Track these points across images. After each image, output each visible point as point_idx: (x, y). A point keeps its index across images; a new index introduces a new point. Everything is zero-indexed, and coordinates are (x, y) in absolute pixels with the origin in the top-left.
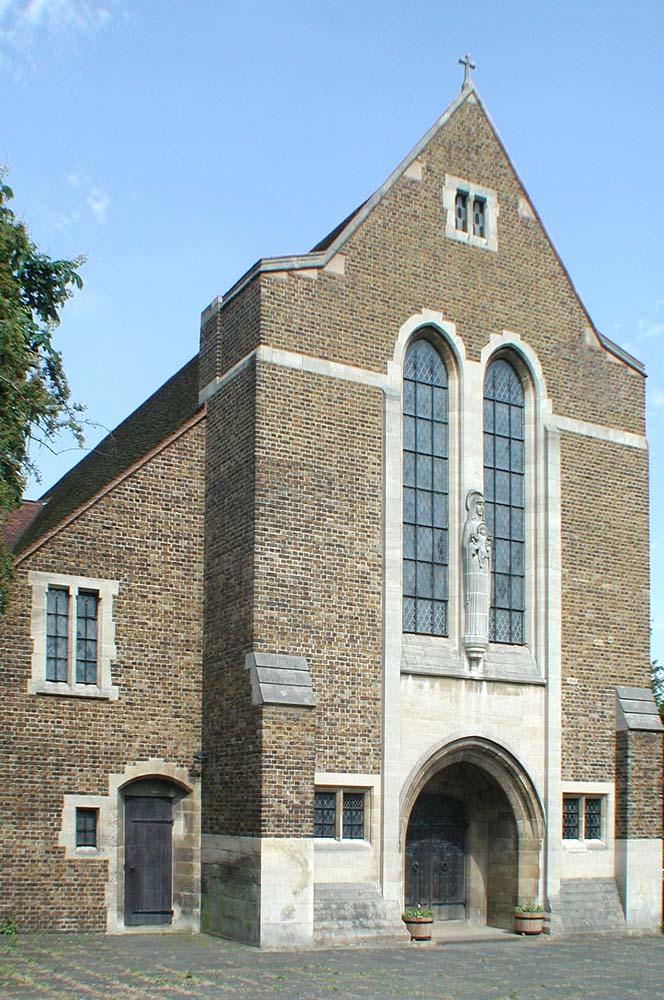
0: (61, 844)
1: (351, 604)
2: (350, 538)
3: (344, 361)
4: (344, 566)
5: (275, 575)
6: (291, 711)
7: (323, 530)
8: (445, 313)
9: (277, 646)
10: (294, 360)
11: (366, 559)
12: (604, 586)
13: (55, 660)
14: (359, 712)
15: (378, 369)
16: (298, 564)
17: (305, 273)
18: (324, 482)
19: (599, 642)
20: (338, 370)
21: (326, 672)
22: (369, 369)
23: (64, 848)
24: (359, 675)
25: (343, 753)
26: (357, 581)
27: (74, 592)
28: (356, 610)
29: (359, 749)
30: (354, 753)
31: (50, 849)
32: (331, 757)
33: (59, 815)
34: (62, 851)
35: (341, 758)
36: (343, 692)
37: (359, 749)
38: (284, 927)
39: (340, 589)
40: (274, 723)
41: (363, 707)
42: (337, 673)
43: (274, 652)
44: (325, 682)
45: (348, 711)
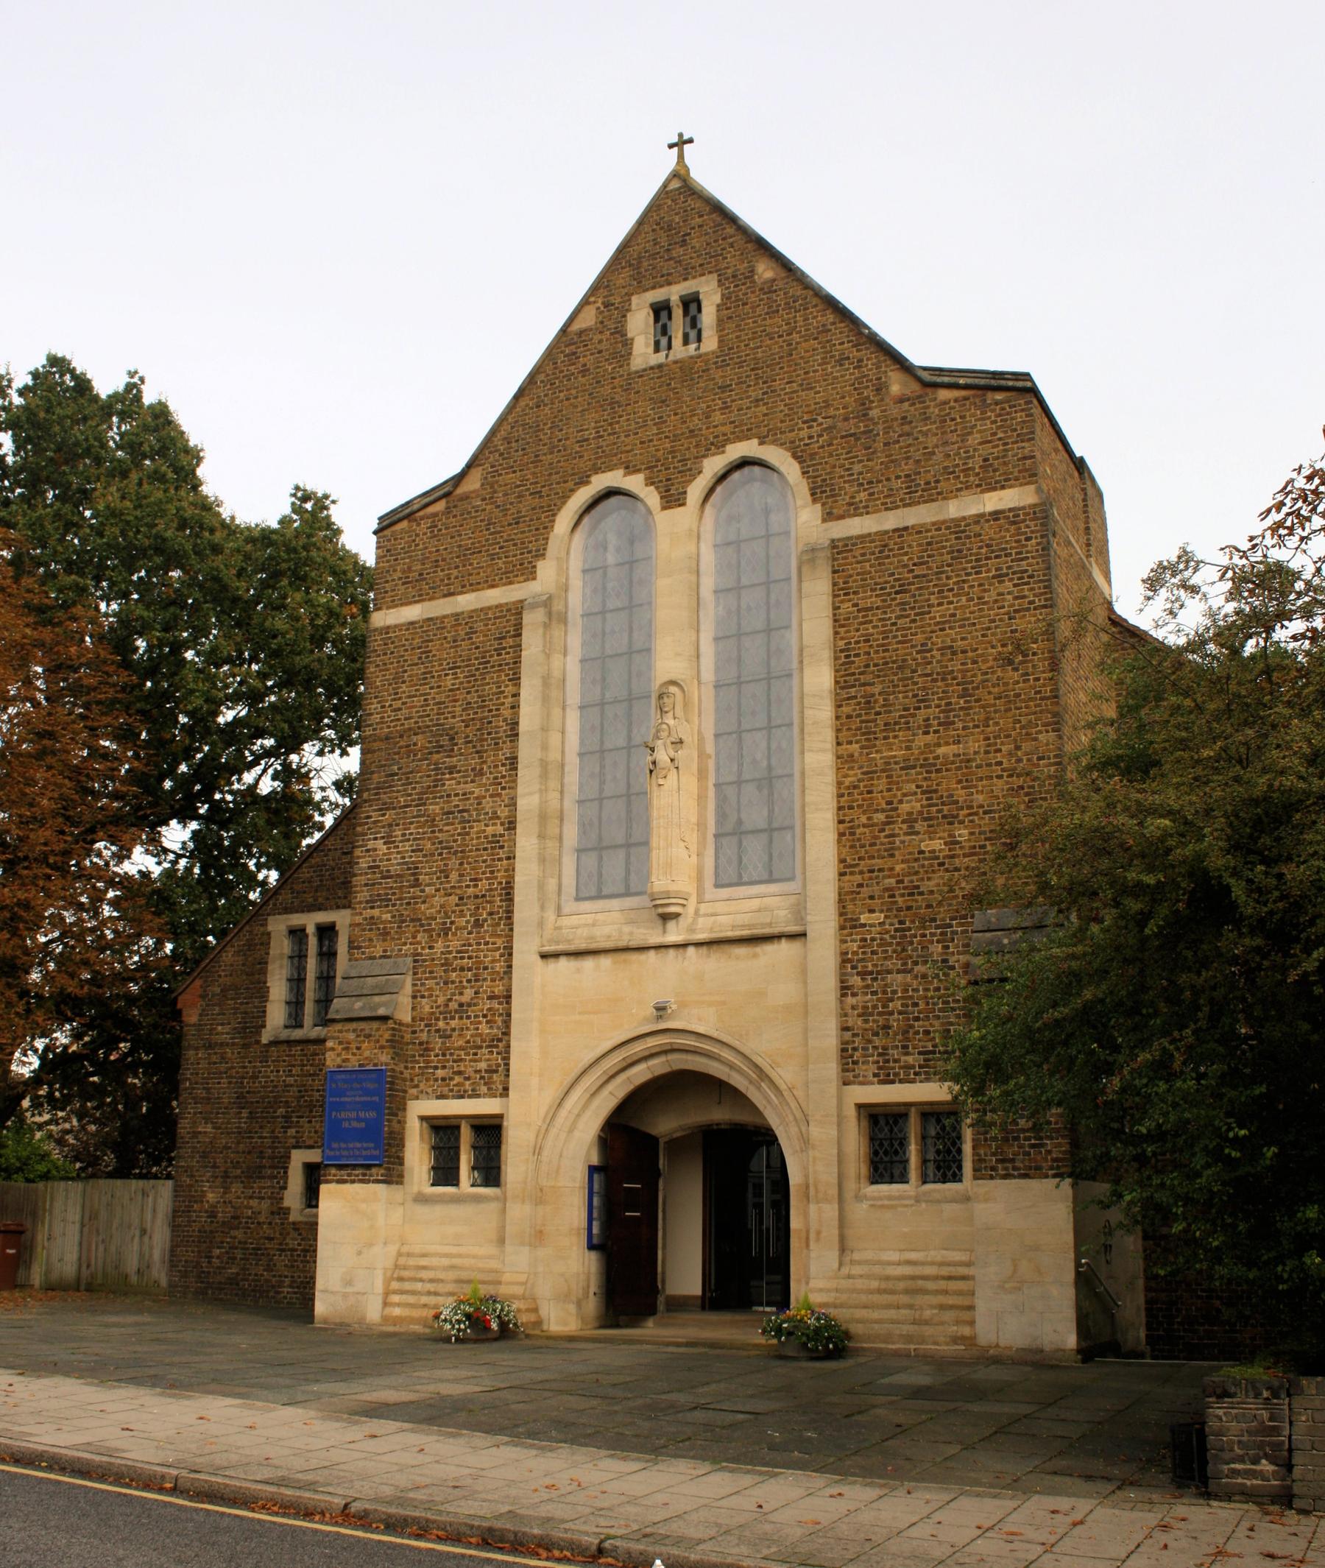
0: (286, 1203)
1: (475, 880)
2: (477, 798)
3: (475, 587)
4: (468, 834)
5: (378, 867)
6: (362, 1025)
7: (442, 797)
8: (627, 468)
9: (378, 951)
10: (412, 613)
11: (498, 818)
12: (941, 751)
13: (296, 1005)
14: (485, 1016)
15: (521, 579)
16: (408, 846)
17: (431, 510)
18: (445, 741)
19: (937, 844)
20: (466, 602)
21: (439, 972)
22: (511, 583)
23: (289, 1209)
24: (486, 968)
25: (460, 1073)
26: (485, 849)
27: (311, 930)
28: (483, 885)
29: (483, 1065)
30: (476, 1072)
31: (275, 1209)
32: (443, 1079)
33: (286, 1173)
34: (287, 1211)
35: (457, 1079)
36: (461, 994)
37: (483, 1065)
38: (345, 1296)
39: (461, 864)
40: (340, 1043)
41: (489, 1009)
42: (454, 970)
43: (374, 958)
44: (437, 984)
45: (468, 1017)
